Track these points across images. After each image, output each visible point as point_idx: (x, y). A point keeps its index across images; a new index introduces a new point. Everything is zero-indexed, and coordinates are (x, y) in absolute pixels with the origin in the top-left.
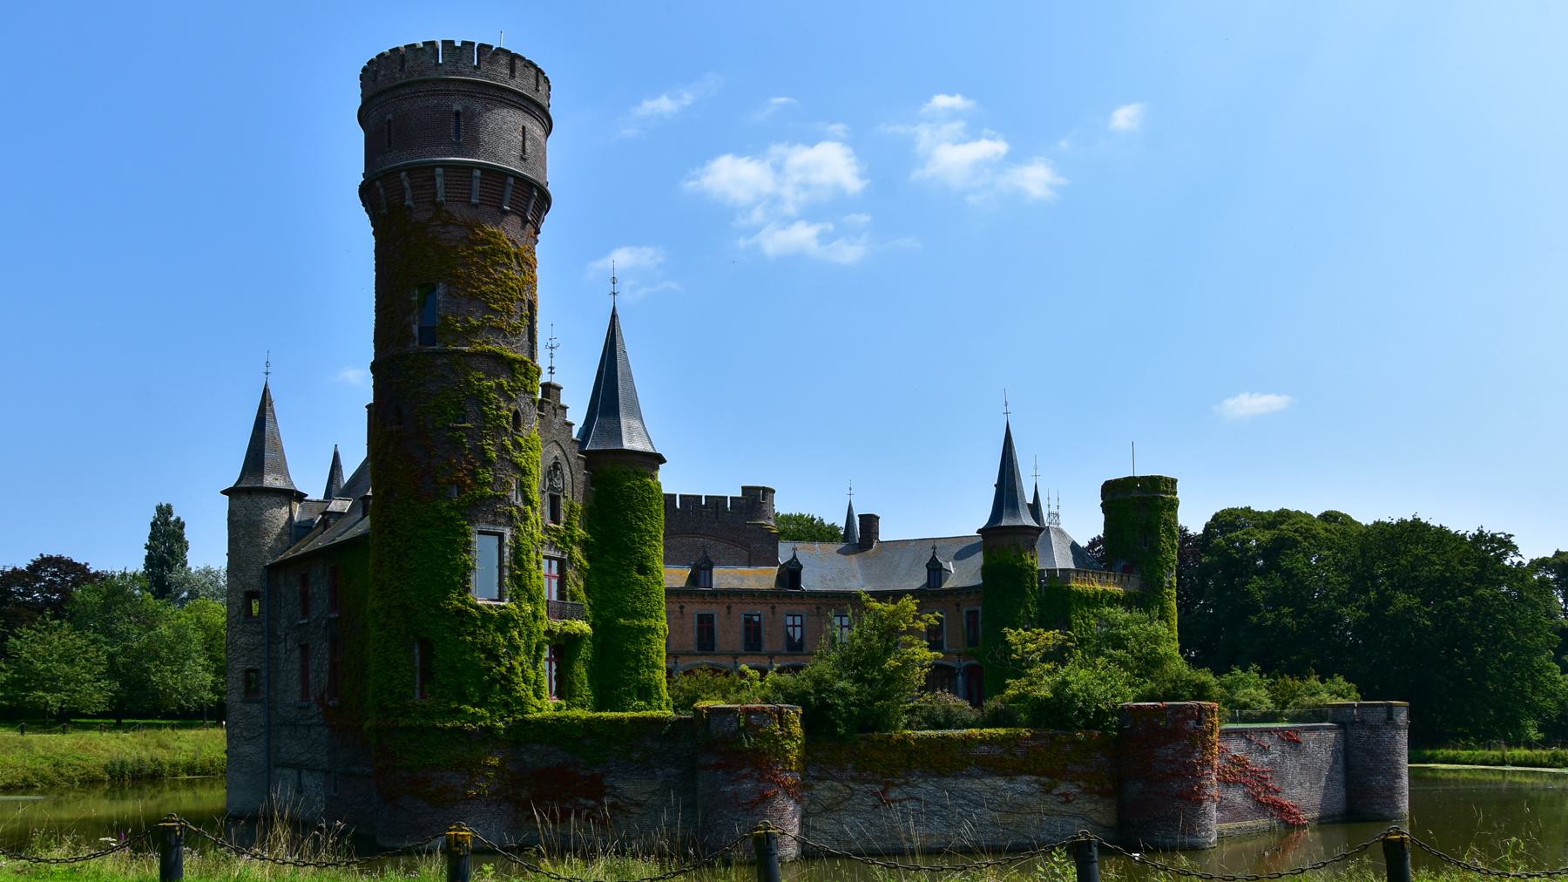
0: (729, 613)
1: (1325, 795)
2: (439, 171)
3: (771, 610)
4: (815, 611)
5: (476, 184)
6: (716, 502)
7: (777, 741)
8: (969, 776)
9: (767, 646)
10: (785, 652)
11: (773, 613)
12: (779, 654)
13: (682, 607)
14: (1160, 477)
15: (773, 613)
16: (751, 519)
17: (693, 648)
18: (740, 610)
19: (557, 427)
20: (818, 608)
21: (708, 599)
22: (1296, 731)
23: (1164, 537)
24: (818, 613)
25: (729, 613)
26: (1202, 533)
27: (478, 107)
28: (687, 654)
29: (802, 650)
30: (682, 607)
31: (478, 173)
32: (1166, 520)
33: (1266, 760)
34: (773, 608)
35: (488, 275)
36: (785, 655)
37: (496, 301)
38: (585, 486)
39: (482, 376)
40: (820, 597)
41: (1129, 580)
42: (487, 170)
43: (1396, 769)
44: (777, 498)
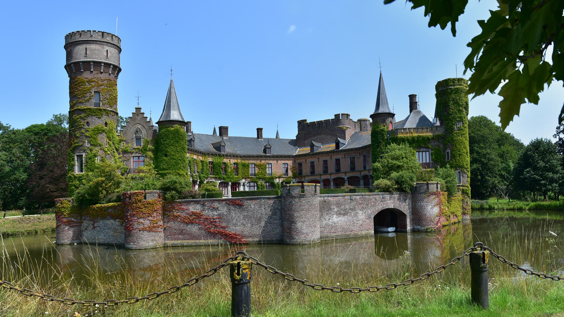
0: (319, 160)
1: (264, 230)
2: (81, 63)
3: (330, 158)
4: (344, 156)
5: (73, 68)
6: (327, 122)
7: (59, 209)
8: (108, 219)
9: (329, 171)
10: (335, 173)
11: (331, 159)
12: (333, 174)
13: (306, 160)
14: (449, 79)
15: (331, 159)
16: (337, 126)
17: (309, 174)
18: (322, 159)
19: (139, 119)
20: (345, 155)
21: (313, 156)
22: (241, 200)
23: (452, 107)
24: (345, 157)
25: (319, 160)
26: (538, 95)
27: (72, 48)
28: (308, 176)
29: (327, 173)
30: (306, 160)
31: (81, 63)
32: (453, 99)
33: (216, 213)
34: (331, 157)
35: (78, 89)
36: (335, 174)
37: (79, 95)
38: (153, 134)
39: (76, 115)
40: (344, 151)
41: (437, 129)
42: (74, 63)
43: (292, 218)
44: (307, 121)
